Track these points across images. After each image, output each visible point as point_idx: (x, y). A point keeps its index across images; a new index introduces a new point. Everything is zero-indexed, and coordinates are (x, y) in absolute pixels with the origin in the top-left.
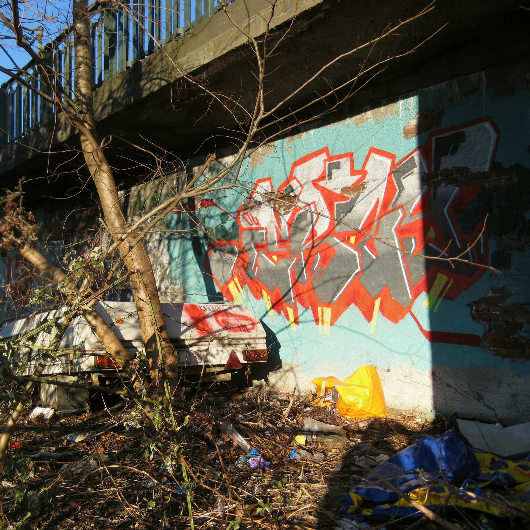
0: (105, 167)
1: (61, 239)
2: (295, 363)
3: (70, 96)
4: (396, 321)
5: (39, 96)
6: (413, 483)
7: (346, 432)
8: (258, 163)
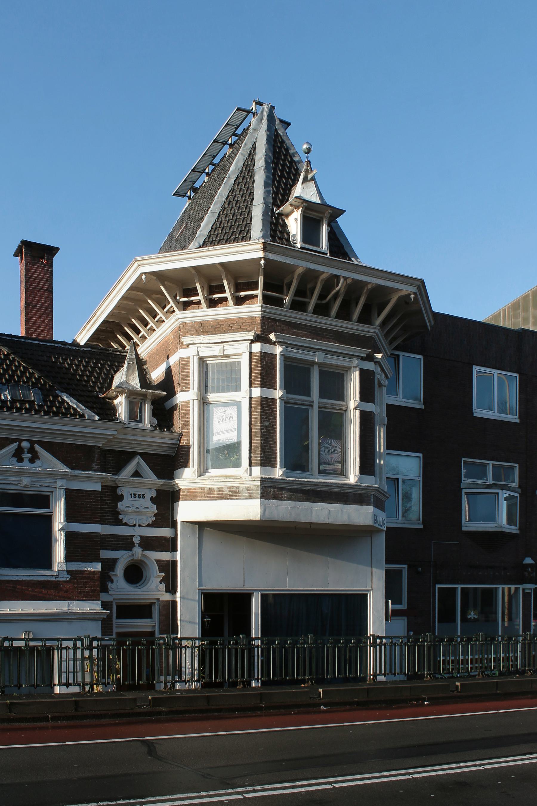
4: (240, 391)
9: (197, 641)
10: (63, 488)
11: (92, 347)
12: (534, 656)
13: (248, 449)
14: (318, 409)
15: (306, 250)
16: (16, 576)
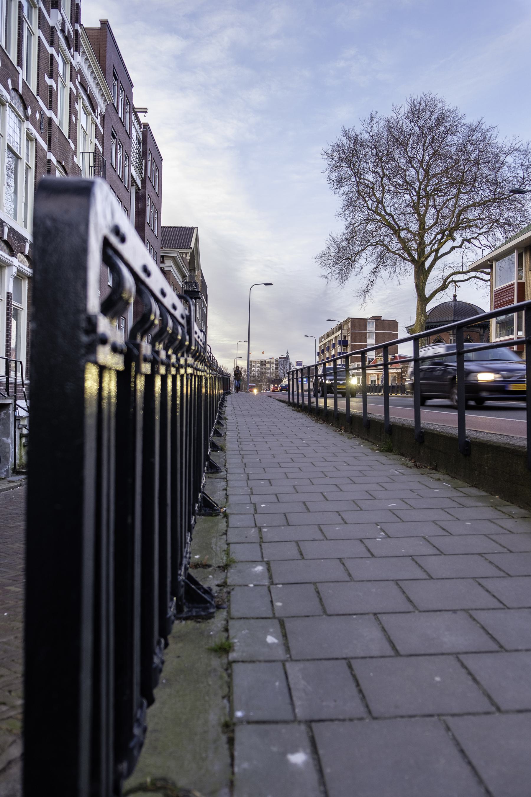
0: (452, 376)
1: (380, 392)
2: (111, 224)
3: (491, 206)
4: (191, 230)
5: (27, 252)
6: (368, 259)
7: (225, 532)
8: (364, 289)
9: (14, 380)
10: (190, 311)
11: (175, 348)
12: (8, 436)
13: (5, 343)
14: (399, 333)
15: (176, 412)
16: (444, 576)
